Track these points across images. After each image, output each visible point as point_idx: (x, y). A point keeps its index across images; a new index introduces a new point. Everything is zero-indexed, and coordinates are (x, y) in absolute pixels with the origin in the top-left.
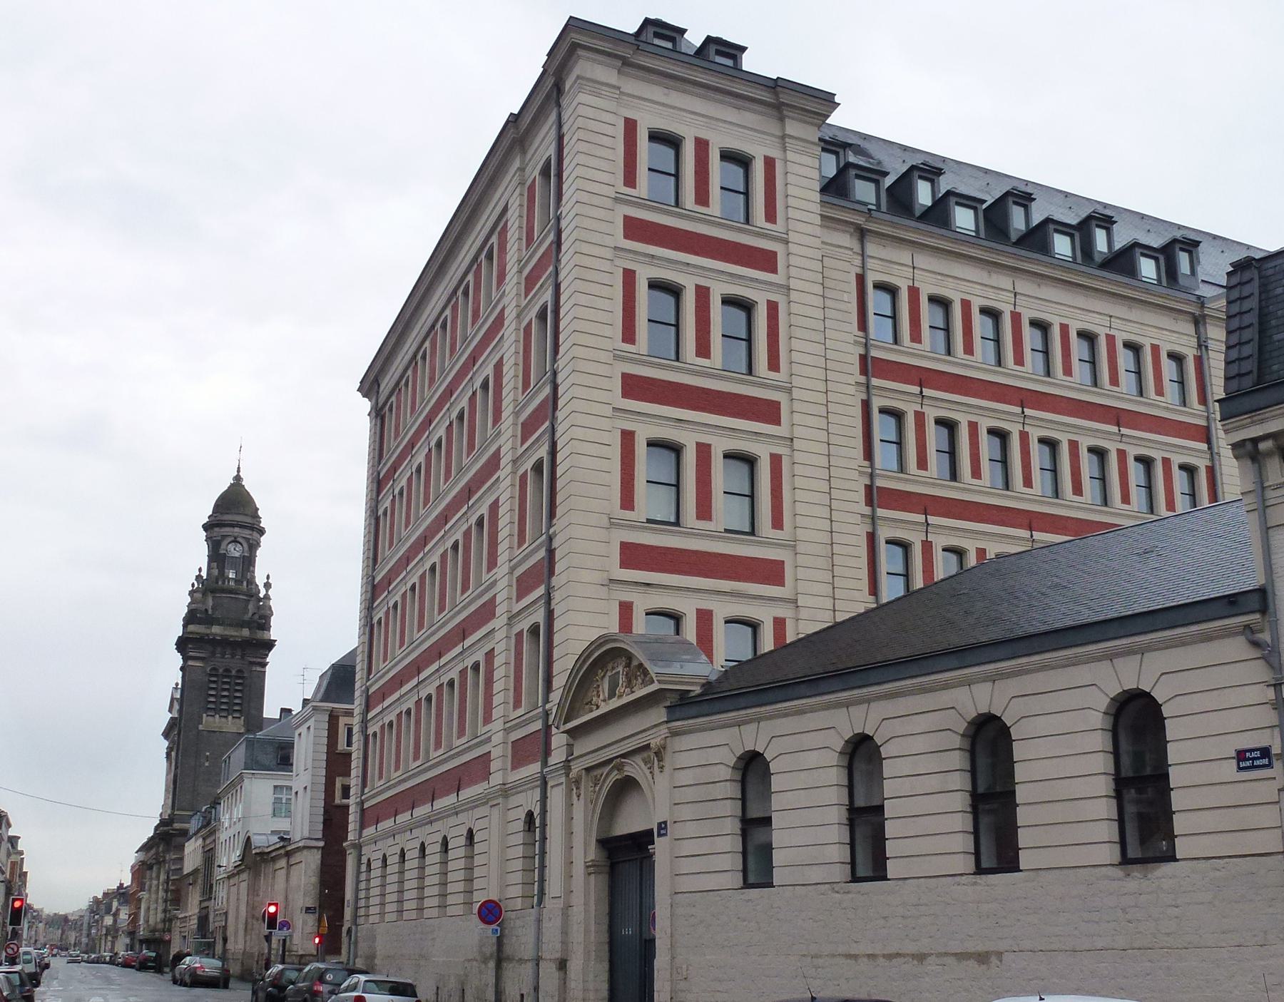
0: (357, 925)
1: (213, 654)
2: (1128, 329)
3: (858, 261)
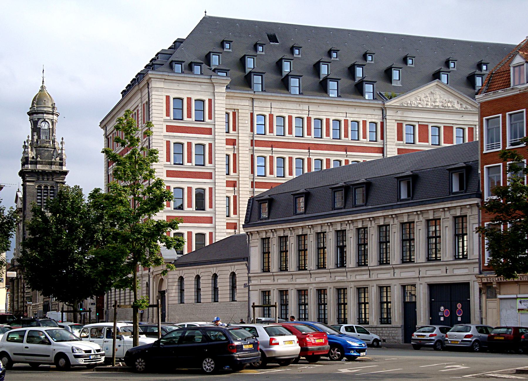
0: (108, 310)
1: (38, 179)
2: (353, 116)
3: (251, 109)
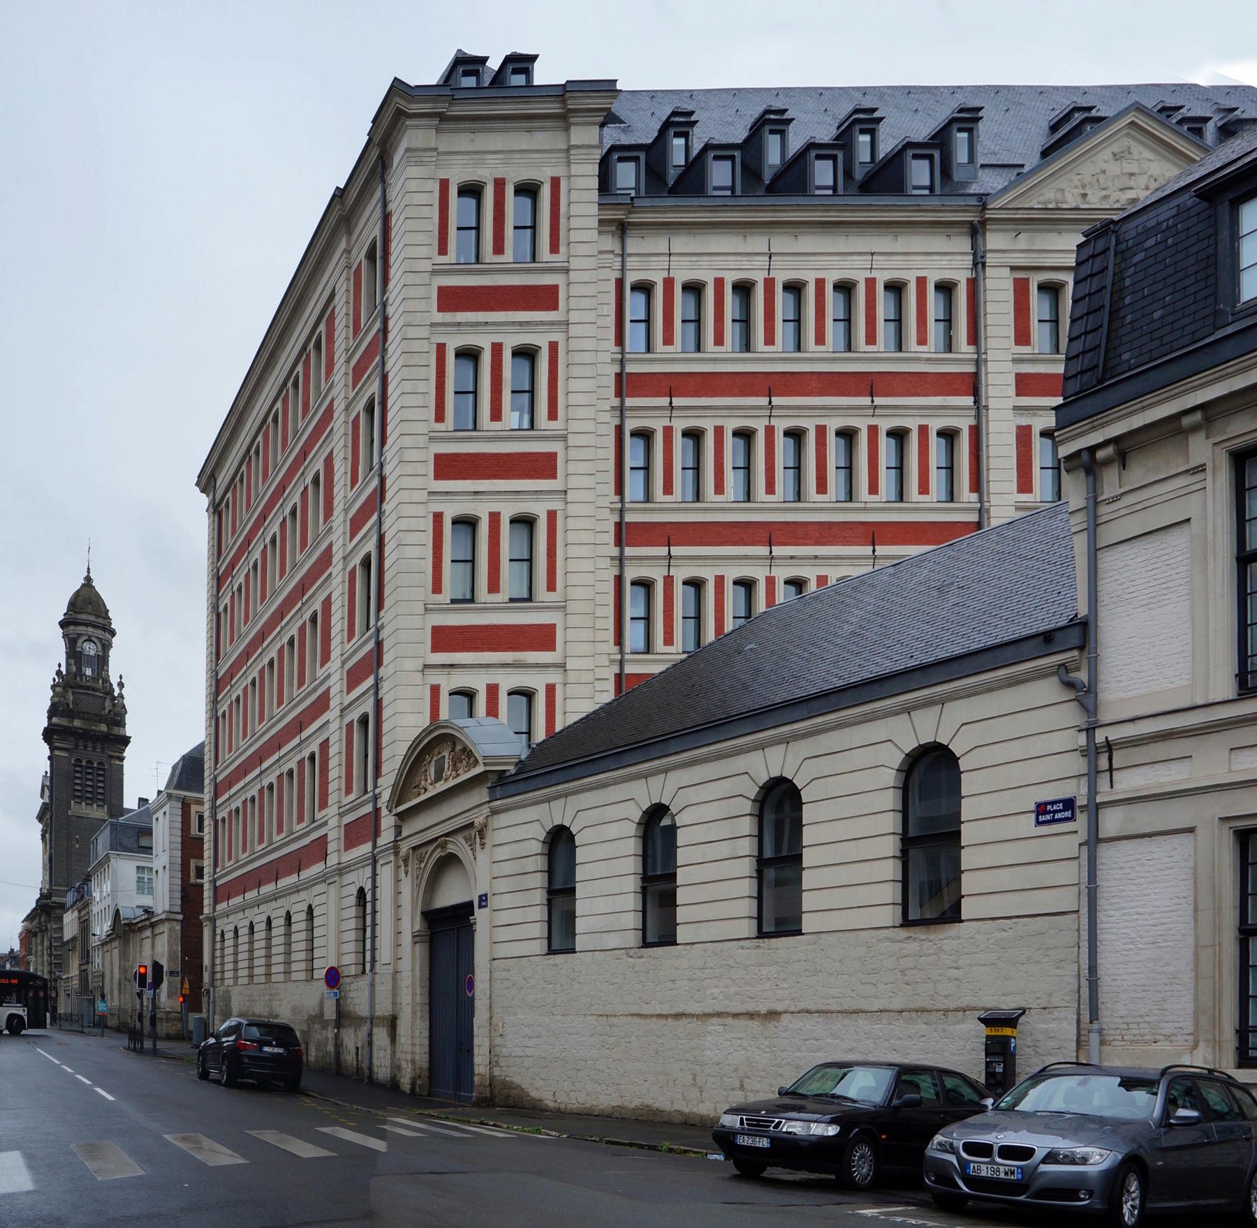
1: (77, 746)
2: (892, 264)
